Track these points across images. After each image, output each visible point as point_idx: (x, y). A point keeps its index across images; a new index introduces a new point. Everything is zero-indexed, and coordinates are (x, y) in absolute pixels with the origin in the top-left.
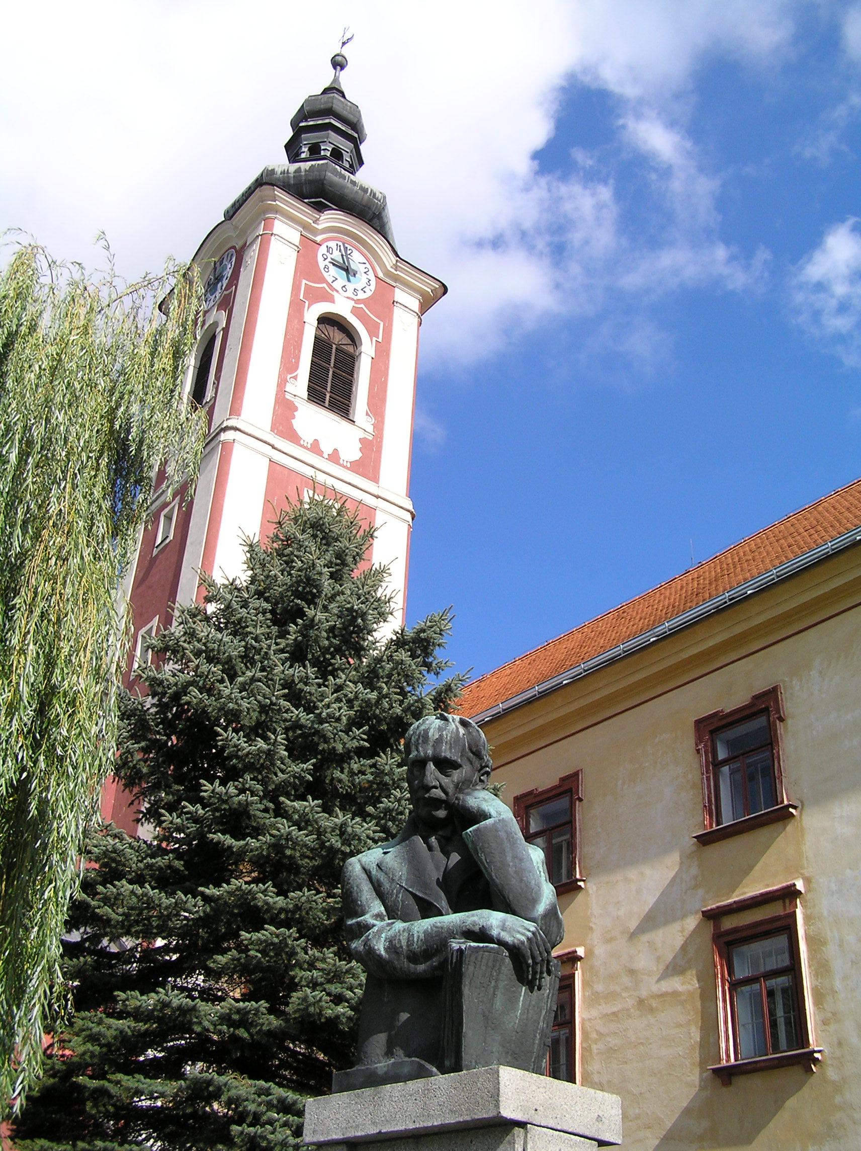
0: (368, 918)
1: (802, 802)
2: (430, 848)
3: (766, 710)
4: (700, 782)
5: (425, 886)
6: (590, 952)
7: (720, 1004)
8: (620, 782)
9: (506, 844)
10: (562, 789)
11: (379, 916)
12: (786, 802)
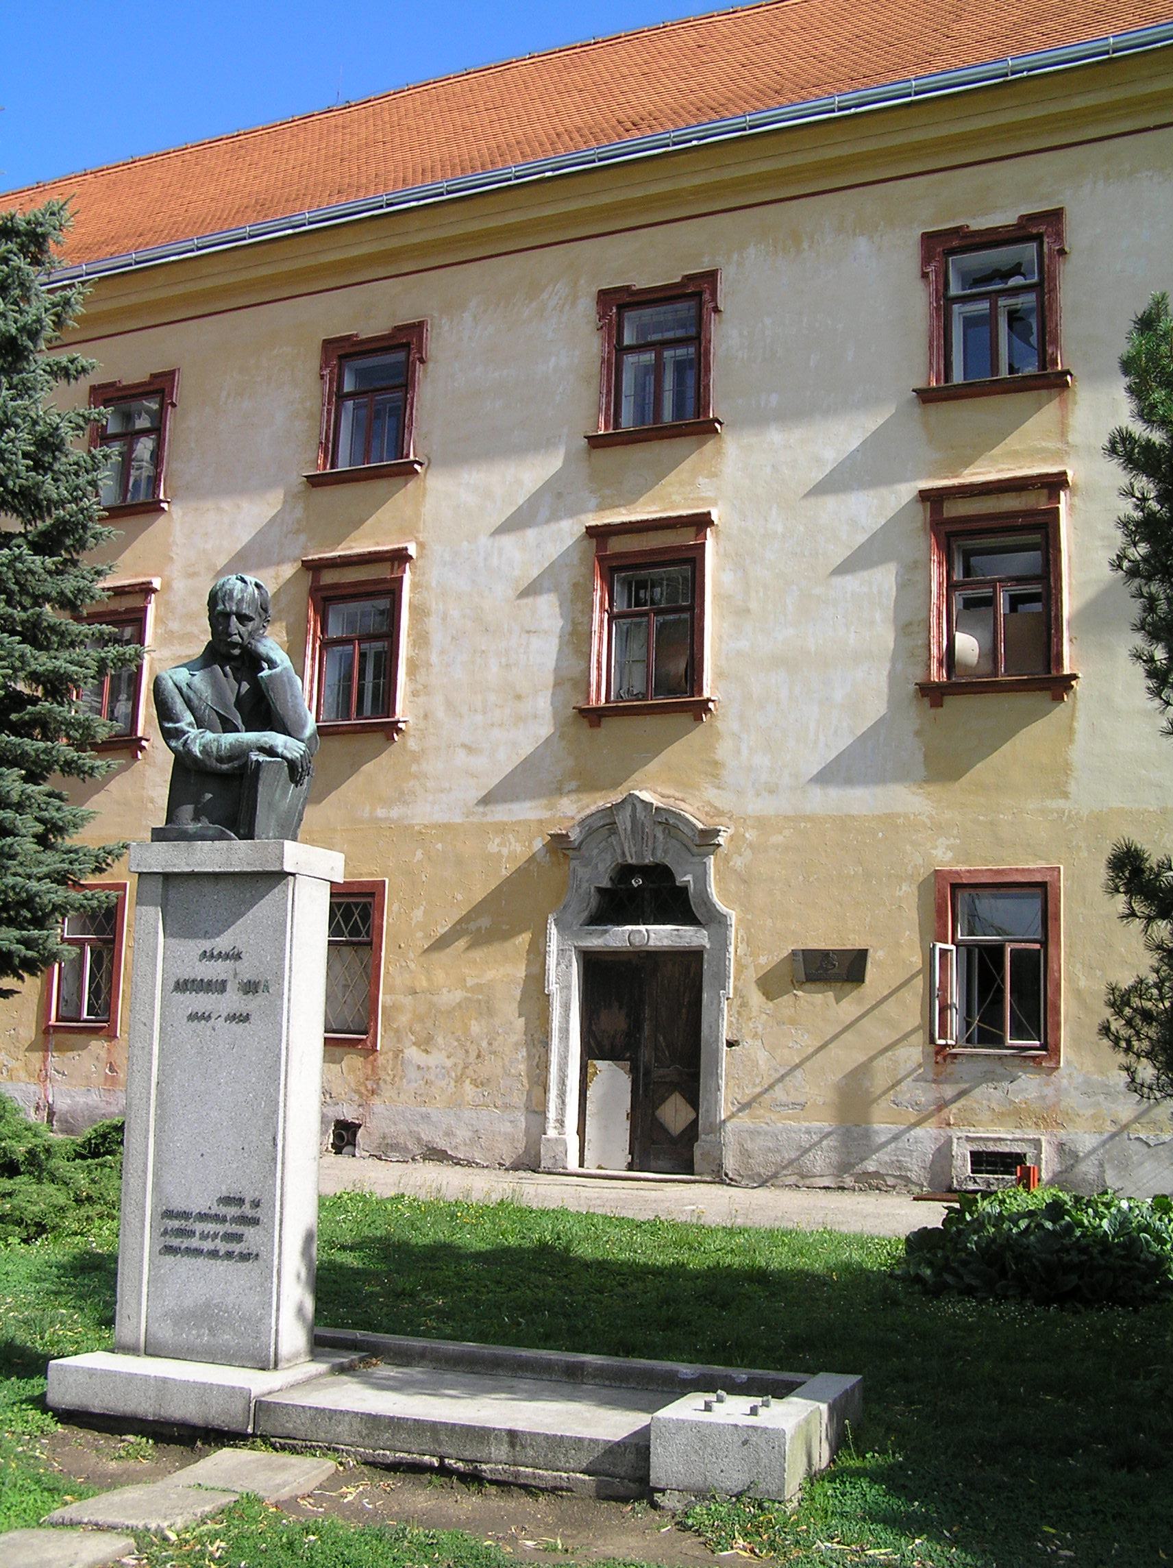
0: (182, 725)
1: (429, 459)
2: (226, 675)
3: (407, 346)
4: (318, 413)
5: (225, 706)
6: (167, 585)
7: (308, 662)
8: (224, 393)
9: (288, 687)
10: (152, 388)
11: (190, 724)
12: (412, 457)
